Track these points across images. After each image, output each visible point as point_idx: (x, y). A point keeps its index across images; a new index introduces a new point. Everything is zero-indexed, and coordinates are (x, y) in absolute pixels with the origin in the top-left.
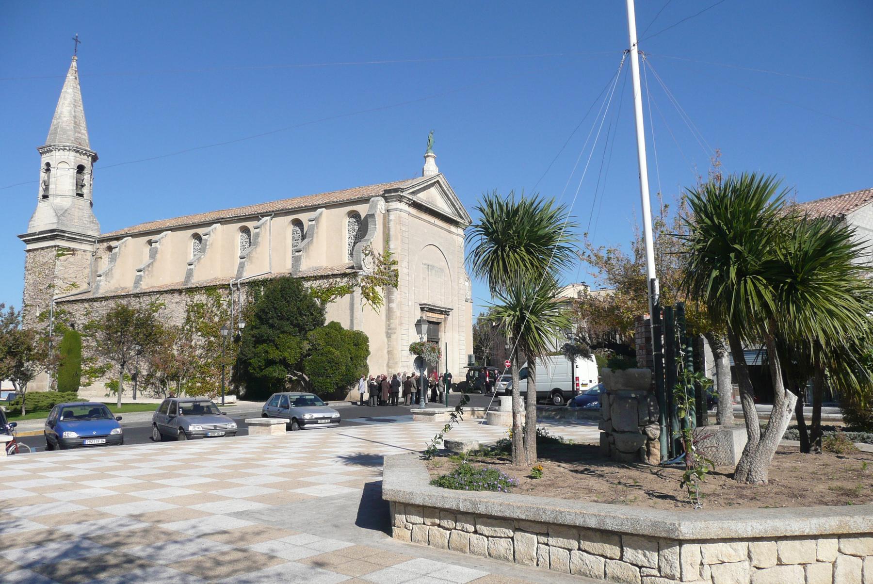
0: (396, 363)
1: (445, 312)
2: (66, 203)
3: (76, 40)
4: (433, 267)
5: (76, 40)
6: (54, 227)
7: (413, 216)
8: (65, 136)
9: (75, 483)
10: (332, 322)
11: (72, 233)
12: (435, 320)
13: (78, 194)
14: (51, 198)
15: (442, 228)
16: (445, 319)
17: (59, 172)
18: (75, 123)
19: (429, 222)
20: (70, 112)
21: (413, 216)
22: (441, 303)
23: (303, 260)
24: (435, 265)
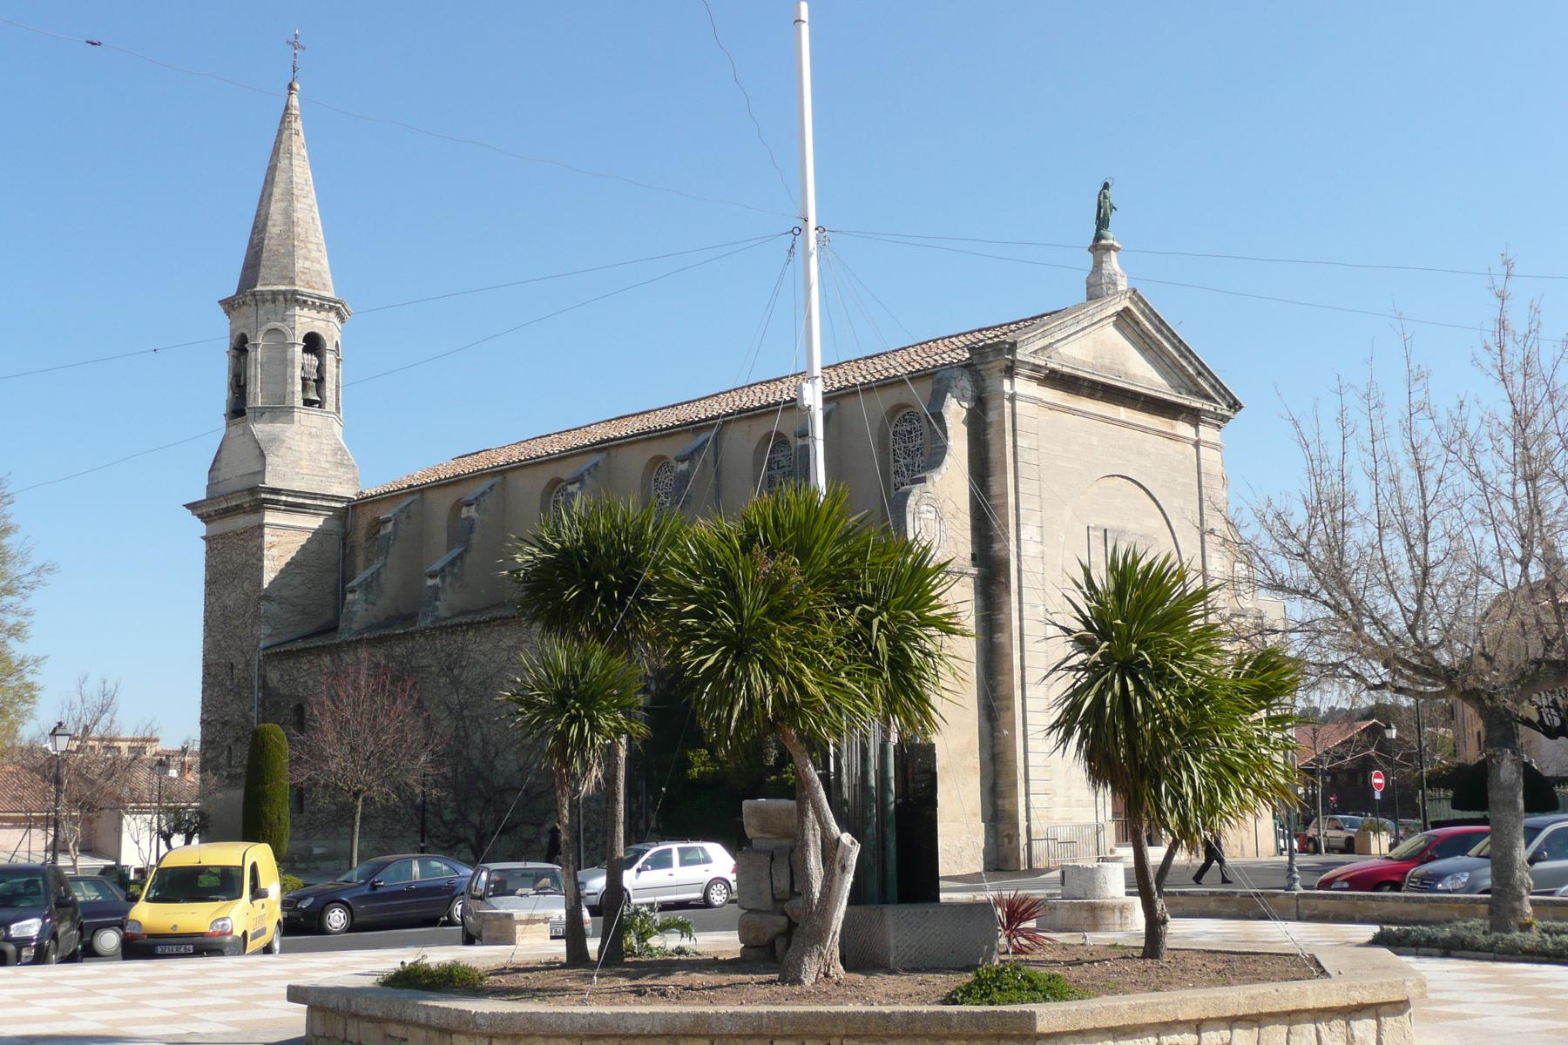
7: (1052, 407)
21: (1052, 407)
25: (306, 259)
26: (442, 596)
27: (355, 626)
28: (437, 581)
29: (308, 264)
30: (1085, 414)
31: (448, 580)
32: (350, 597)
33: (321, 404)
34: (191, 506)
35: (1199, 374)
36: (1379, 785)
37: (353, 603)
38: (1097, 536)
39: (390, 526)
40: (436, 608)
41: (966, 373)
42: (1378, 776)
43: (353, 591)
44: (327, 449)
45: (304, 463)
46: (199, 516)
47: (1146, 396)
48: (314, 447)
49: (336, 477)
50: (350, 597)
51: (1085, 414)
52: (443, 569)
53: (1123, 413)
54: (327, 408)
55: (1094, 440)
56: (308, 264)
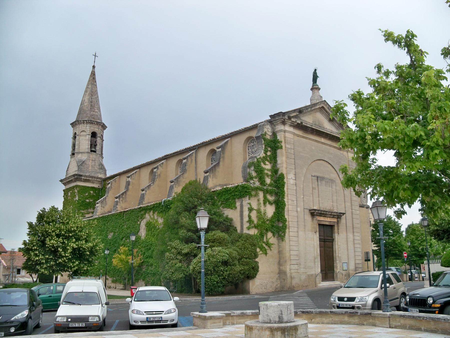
0: (286, 261)
1: (339, 216)
2: (84, 157)
3: (95, 56)
4: (323, 178)
5: (95, 56)
6: (76, 173)
7: (298, 136)
8: (85, 115)
9: (251, 323)
10: (409, 226)
11: (86, 176)
12: (327, 223)
13: (91, 151)
14: (76, 155)
15: (330, 146)
16: (338, 223)
17: (81, 138)
18: (91, 105)
19: (313, 140)
20: (89, 99)
21: (298, 136)
22: (361, 208)
23: (210, 179)
24: (326, 176)
25: (94, 112)
26: (119, 204)
27: (98, 214)
28: (118, 199)
29: (94, 113)
30: (310, 139)
31: (121, 199)
32: (97, 205)
33: (95, 152)
34: (61, 181)
35: (228, 315)
36: (405, 256)
37: (98, 207)
38: (98, 152)
39: (110, 185)
40: (117, 207)
41: (269, 124)
42: (405, 253)
43: (98, 203)
44: (97, 164)
45: (90, 168)
46: (63, 184)
47: (330, 135)
48: (93, 163)
49: (99, 172)
50: (97, 205)
51: (310, 139)
52: (119, 196)
53: (323, 140)
54: (97, 152)
55: (313, 148)
56: (94, 113)
